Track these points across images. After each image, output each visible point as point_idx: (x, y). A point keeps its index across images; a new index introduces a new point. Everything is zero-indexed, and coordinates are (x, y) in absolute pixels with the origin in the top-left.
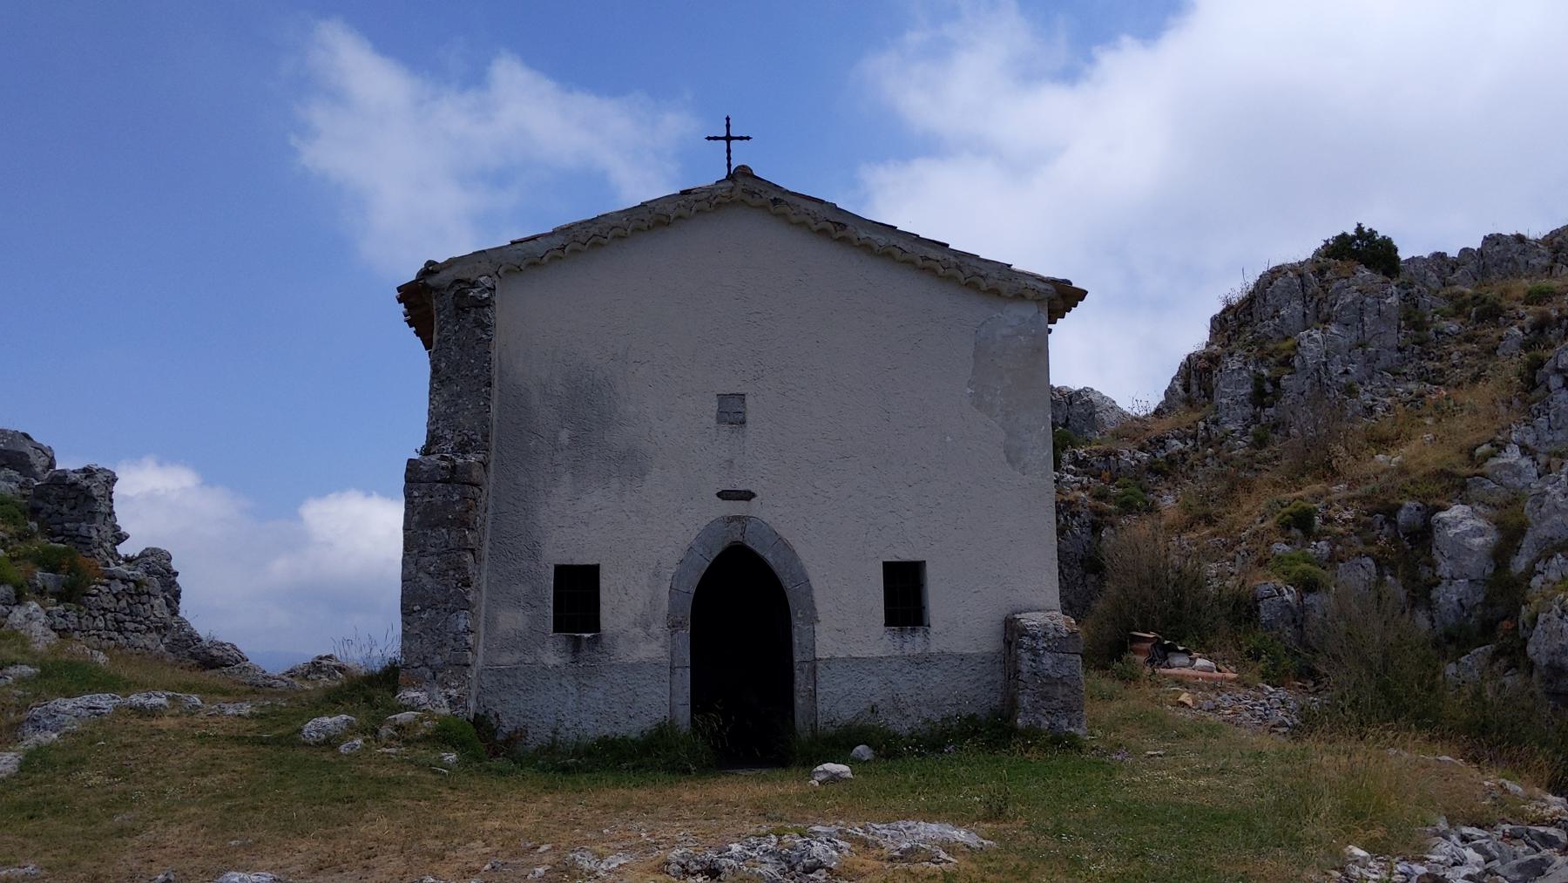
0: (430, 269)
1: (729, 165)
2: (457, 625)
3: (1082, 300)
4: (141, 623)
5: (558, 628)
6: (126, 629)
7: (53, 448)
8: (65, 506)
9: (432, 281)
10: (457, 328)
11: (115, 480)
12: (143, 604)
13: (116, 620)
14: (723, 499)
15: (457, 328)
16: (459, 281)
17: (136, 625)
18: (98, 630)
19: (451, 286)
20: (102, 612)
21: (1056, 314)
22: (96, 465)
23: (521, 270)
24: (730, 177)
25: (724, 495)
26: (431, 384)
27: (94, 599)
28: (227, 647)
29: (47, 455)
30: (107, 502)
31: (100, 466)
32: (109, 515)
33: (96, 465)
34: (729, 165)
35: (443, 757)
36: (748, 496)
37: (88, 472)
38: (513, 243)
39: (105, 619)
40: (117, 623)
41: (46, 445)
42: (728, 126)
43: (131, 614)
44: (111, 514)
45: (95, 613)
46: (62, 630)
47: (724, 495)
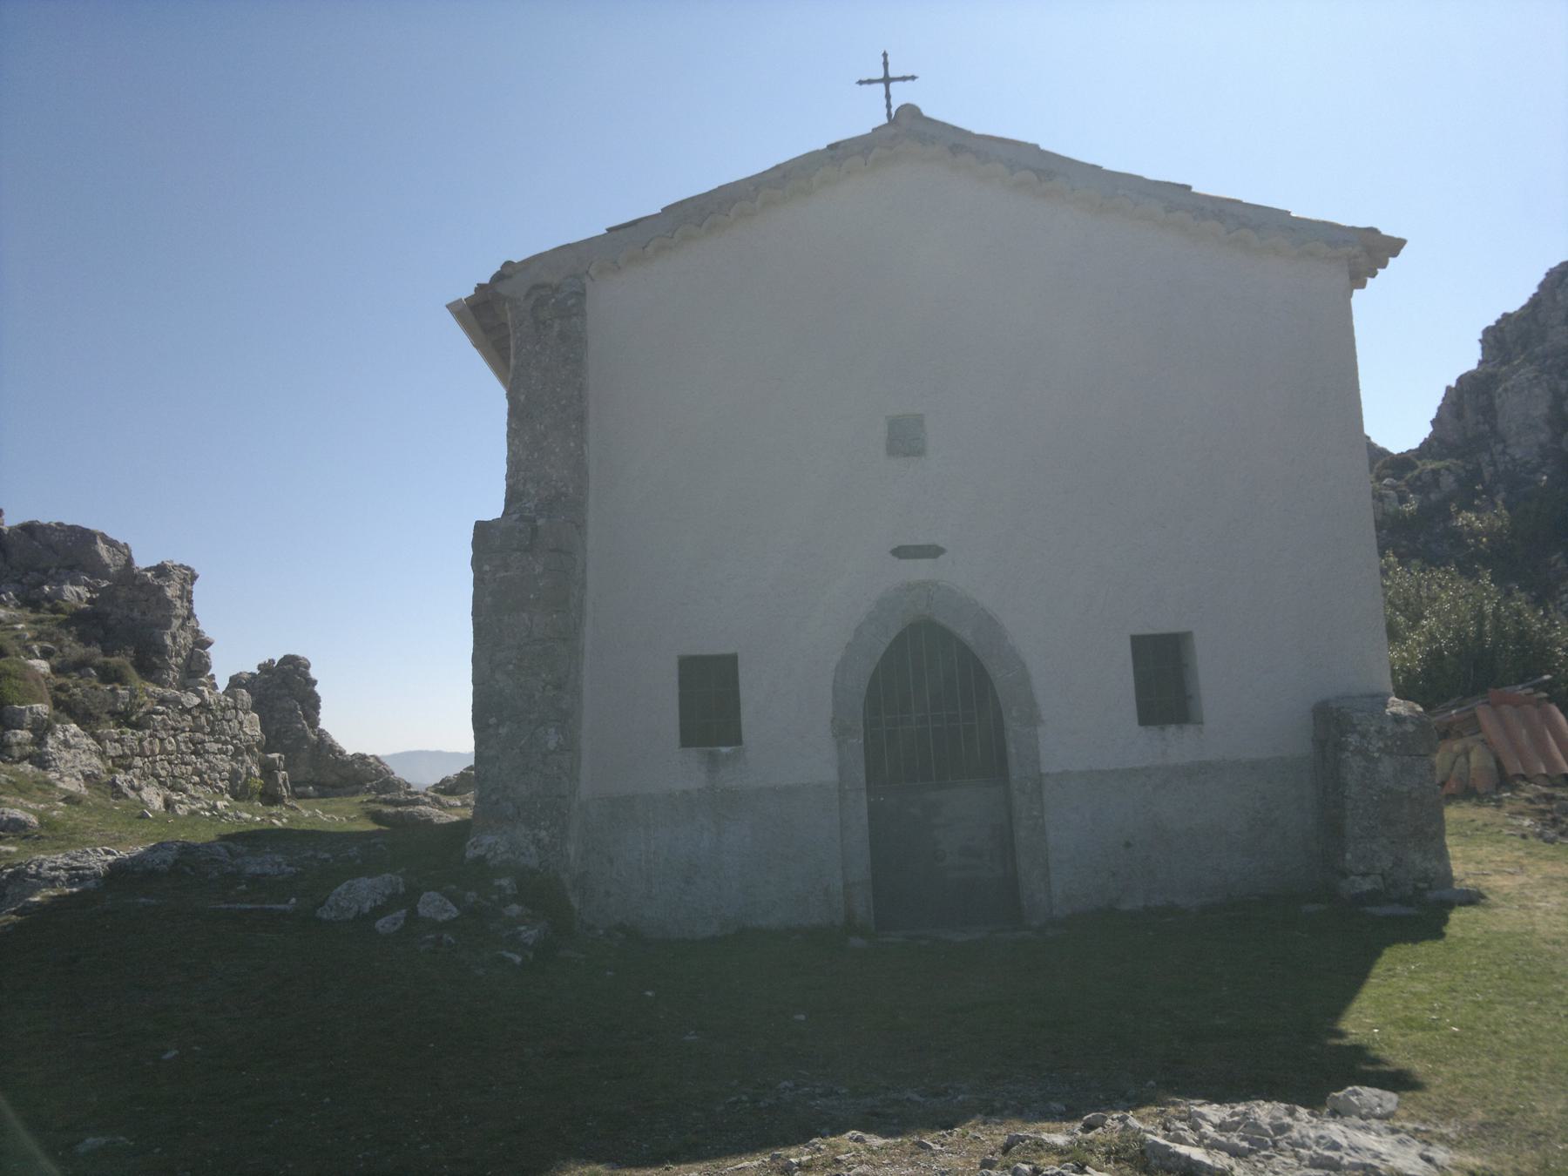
0: (507, 272)
1: (889, 106)
2: (547, 743)
3: (1395, 255)
4: (225, 743)
5: (687, 740)
6: (208, 752)
7: (130, 545)
8: (136, 610)
9: (503, 289)
10: (537, 348)
11: (194, 578)
12: (229, 721)
13: (191, 741)
14: (900, 558)
15: (537, 348)
16: (536, 287)
17: (220, 746)
18: (168, 755)
19: (528, 296)
20: (172, 732)
21: (1358, 280)
22: (172, 561)
23: (619, 268)
24: (893, 120)
25: (901, 552)
26: (509, 424)
27: (160, 718)
28: (371, 760)
29: (123, 553)
30: (186, 604)
31: (177, 563)
32: (189, 619)
33: (172, 561)
34: (889, 106)
35: (520, 933)
36: (933, 552)
37: (161, 570)
38: (609, 230)
39: (177, 741)
40: (194, 745)
41: (121, 541)
42: (886, 64)
43: (212, 733)
44: (191, 615)
45: (163, 734)
46: (117, 757)
47: (901, 552)
